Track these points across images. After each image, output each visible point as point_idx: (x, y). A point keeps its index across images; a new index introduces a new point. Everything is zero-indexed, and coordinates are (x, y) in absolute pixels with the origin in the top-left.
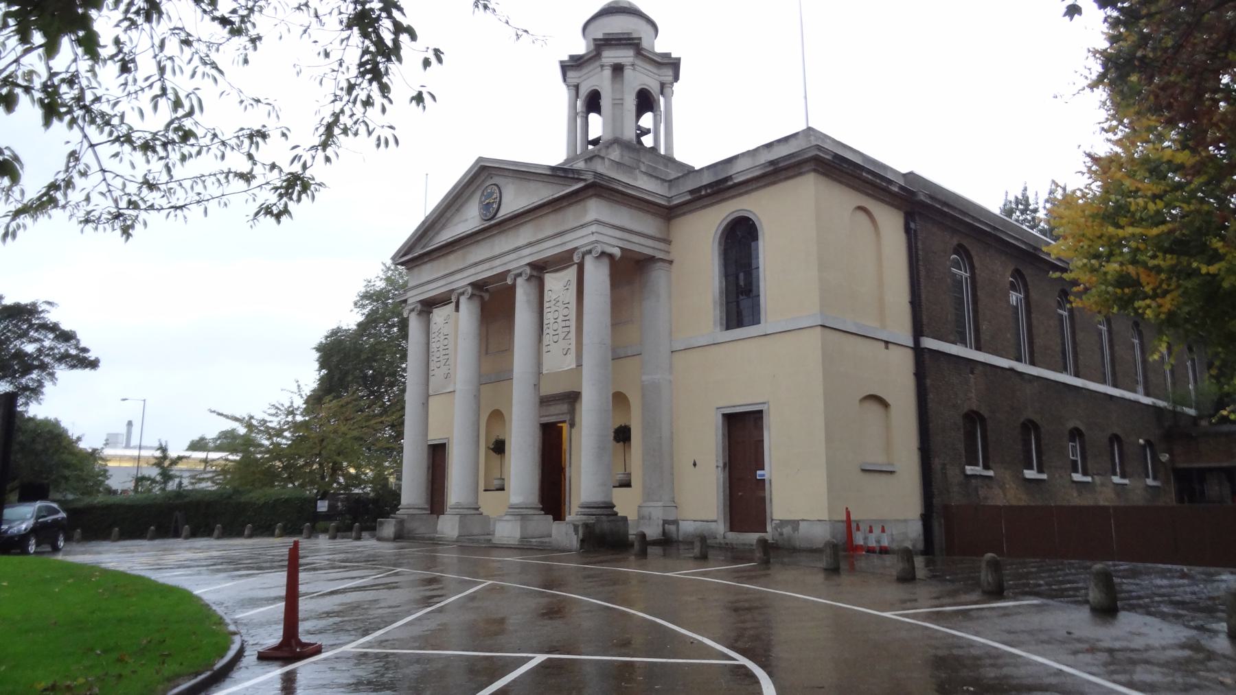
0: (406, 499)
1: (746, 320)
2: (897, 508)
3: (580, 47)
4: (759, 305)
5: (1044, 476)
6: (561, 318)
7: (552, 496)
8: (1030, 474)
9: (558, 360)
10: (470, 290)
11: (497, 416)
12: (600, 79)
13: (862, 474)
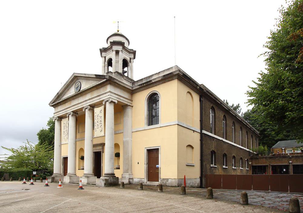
0: (54, 172)
1: (153, 123)
2: (194, 175)
3: (106, 46)
4: (159, 119)
5: (227, 167)
6: (99, 121)
7: (97, 171)
8: (224, 167)
9: (98, 133)
10: (72, 113)
11: (82, 150)
12: (111, 55)
13: (186, 166)
